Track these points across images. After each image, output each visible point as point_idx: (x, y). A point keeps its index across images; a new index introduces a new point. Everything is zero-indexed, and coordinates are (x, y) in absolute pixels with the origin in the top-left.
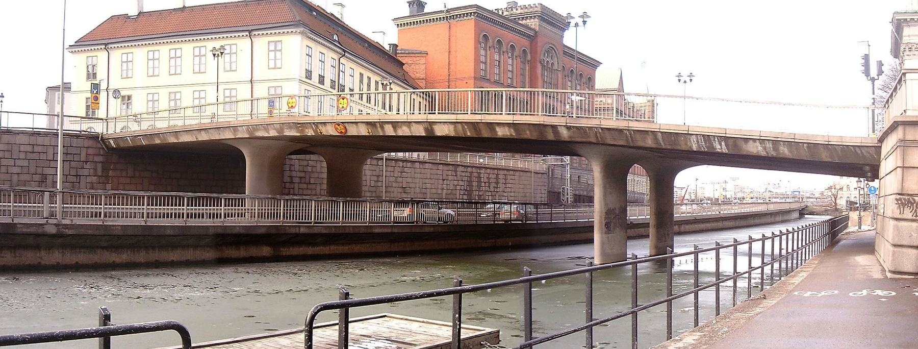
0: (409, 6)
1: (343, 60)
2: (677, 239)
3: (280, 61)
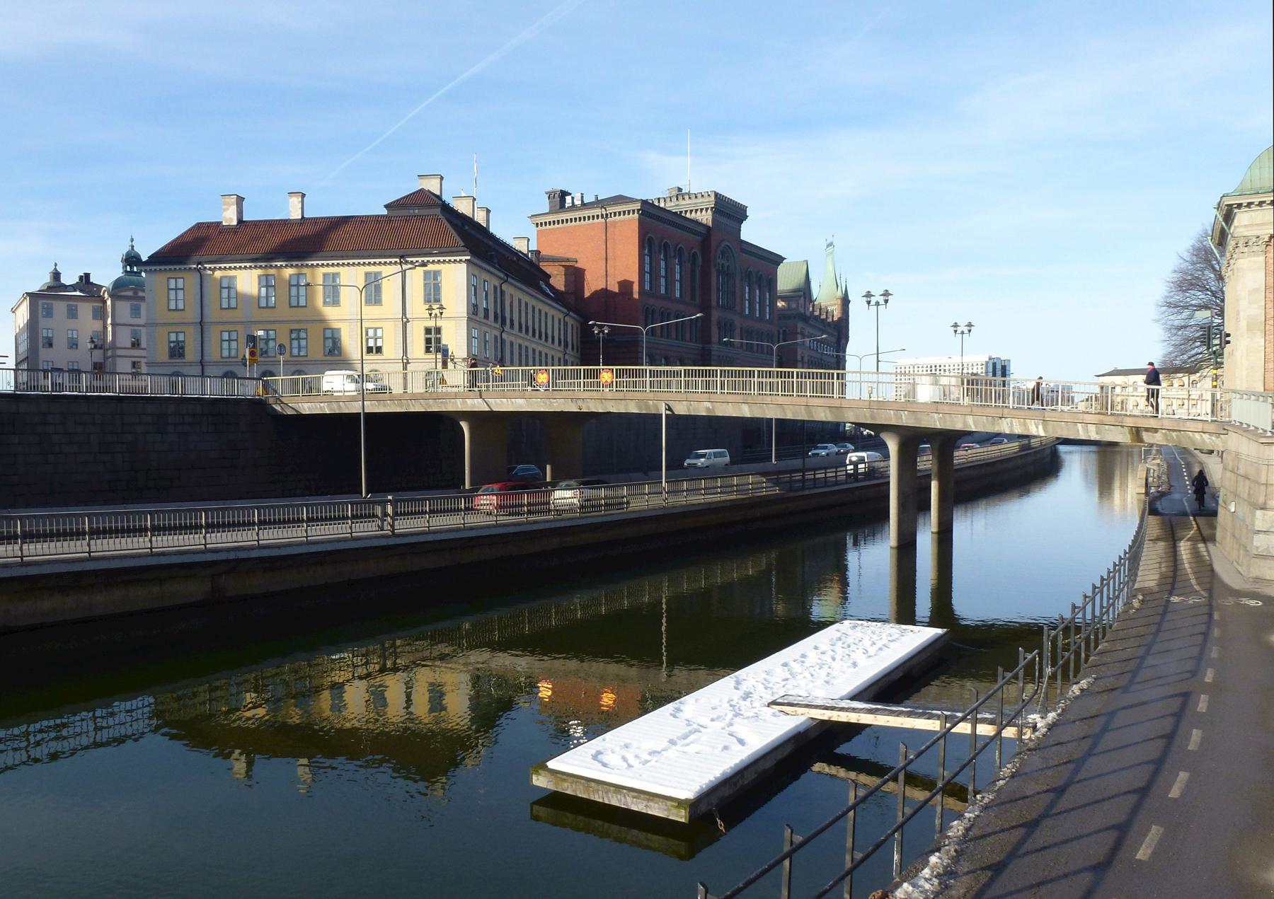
0: (549, 198)
1: (504, 287)
2: (1213, 669)
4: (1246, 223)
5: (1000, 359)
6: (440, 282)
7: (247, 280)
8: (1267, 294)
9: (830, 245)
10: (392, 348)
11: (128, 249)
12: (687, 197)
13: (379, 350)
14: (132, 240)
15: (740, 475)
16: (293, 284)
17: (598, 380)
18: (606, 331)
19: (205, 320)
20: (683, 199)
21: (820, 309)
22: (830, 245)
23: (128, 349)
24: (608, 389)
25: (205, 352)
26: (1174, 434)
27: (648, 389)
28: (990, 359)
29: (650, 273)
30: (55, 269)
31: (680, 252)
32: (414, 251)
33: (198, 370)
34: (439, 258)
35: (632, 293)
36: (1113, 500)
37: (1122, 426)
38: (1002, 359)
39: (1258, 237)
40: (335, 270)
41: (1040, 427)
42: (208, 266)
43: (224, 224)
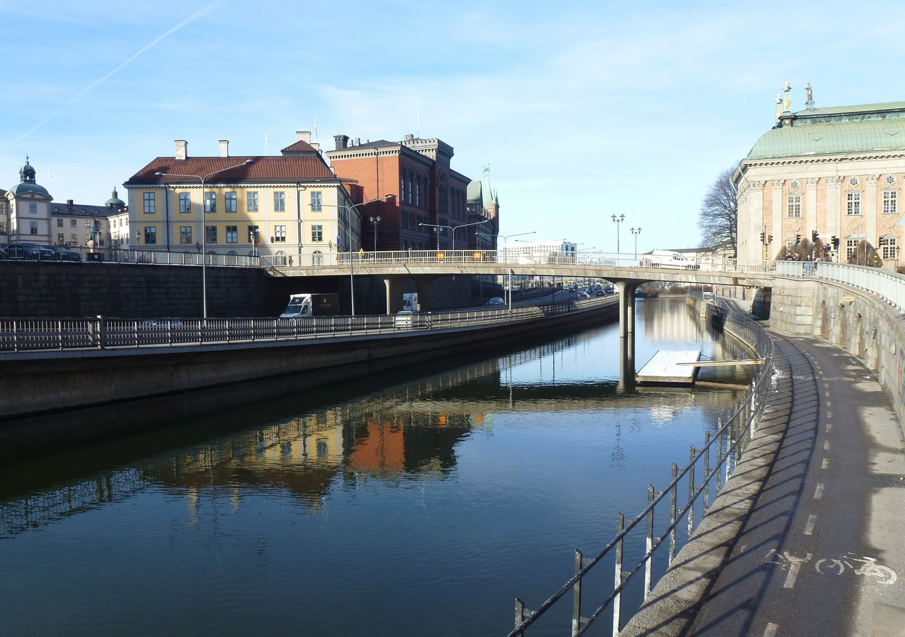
0: (336, 140)
3: (146, 205)
4: (754, 174)
5: (570, 243)
6: (321, 199)
7: (197, 195)
8: (764, 212)
9: (487, 170)
10: (291, 237)
11: (24, 164)
12: (420, 142)
13: (283, 239)
14: (28, 158)
15: (486, 311)
16: (229, 198)
17: (473, 257)
18: (441, 230)
19: (169, 220)
20: (418, 143)
21: (485, 212)
22: (487, 170)
23: (29, 235)
24: (442, 262)
25: (170, 239)
26: (752, 280)
27: (463, 262)
28: (564, 243)
29: (404, 190)
30: (115, 190)
31: (419, 176)
32: (305, 180)
33: (167, 250)
34: (321, 184)
35: (395, 203)
36: (653, 331)
37: (730, 277)
38: (572, 243)
39: (759, 182)
40: (255, 190)
41: (694, 278)
42: (171, 186)
43: (177, 159)
